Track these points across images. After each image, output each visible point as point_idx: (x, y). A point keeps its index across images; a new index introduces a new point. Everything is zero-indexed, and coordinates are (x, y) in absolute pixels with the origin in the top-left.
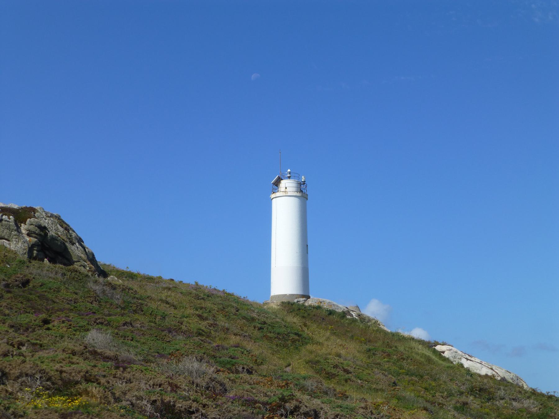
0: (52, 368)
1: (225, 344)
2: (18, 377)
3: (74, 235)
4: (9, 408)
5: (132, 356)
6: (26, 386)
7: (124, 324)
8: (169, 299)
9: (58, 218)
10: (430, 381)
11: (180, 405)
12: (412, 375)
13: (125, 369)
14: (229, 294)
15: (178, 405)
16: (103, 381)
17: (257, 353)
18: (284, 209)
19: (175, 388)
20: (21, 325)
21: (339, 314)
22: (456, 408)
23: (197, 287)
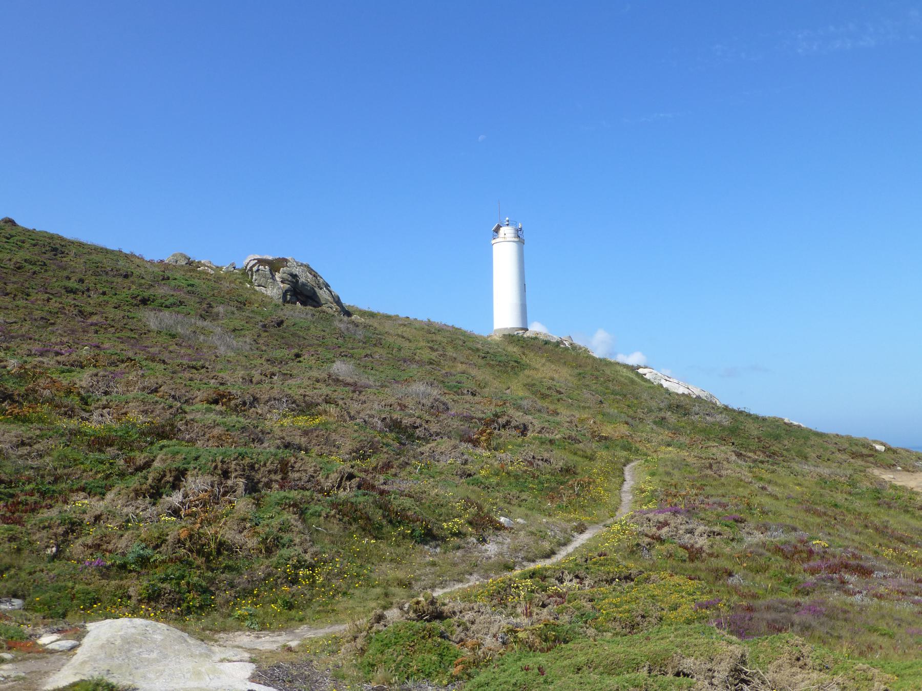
0: (296, 393)
1: (453, 371)
2: (267, 402)
3: (321, 281)
4: (257, 427)
5: (371, 383)
6: (275, 408)
7: (366, 356)
8: (405, 334)
9: (307, 266)
10: (632, 400)
11: (406, 421)
12: (616, 394)
13: (360, 392)
14: (457, 329)
15: (404, 421)
16: (341, 402)
17: (481, 378)
18: (504, 252)
19: (403, 407)
20: (276, 359)
21: (554, 343)
22: (655, 423)
23: (430, 323)
